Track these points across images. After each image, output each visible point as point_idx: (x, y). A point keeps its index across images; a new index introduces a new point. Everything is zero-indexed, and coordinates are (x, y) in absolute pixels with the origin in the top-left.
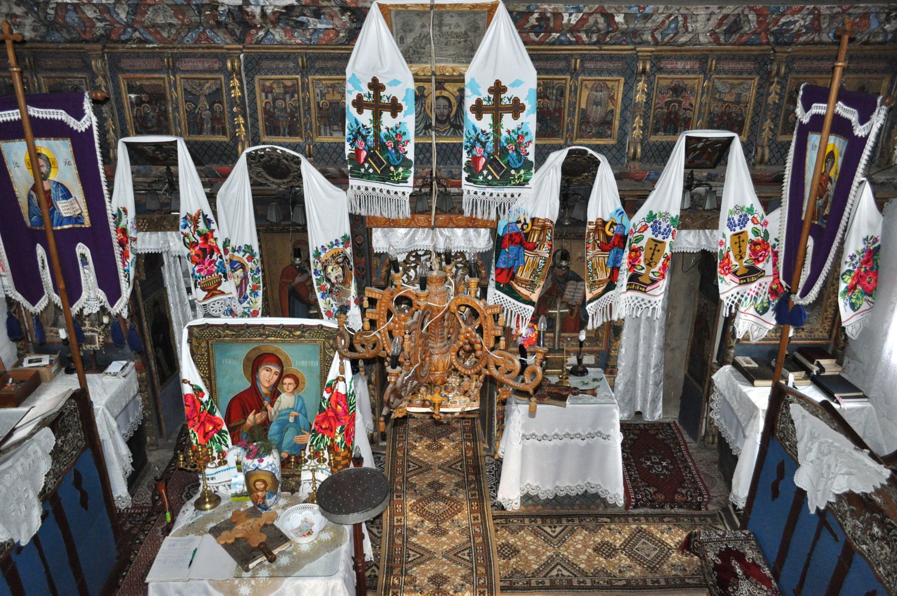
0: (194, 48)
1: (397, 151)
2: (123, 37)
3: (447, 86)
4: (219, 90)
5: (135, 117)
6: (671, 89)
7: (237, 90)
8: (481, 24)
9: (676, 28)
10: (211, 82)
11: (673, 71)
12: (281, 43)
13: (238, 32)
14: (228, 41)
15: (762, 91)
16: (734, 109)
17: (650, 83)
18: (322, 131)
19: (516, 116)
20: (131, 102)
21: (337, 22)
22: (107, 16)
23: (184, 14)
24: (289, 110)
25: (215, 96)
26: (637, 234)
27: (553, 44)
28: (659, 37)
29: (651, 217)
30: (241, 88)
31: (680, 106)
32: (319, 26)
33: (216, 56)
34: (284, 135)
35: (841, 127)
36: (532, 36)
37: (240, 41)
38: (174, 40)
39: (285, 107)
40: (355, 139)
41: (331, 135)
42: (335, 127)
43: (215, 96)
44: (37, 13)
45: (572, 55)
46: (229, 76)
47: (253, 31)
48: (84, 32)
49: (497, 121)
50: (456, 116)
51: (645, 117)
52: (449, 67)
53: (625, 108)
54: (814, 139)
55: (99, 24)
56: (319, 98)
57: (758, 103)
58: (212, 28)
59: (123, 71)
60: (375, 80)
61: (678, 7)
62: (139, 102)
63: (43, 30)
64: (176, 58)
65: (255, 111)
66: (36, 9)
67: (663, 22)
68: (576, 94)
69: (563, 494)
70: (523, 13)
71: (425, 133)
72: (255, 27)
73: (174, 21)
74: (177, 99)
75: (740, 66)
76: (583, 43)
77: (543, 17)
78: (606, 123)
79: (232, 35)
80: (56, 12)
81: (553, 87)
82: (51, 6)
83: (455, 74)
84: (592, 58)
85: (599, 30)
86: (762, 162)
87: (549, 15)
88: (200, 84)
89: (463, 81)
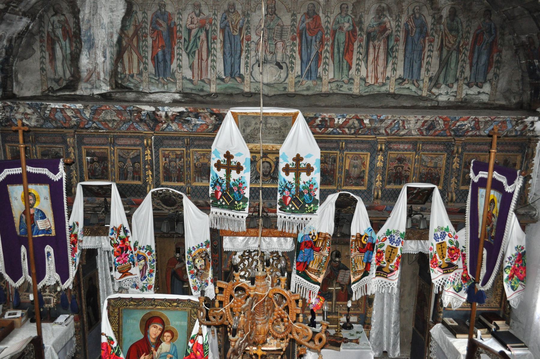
1: (239, 193)
2: (86, 126)
3: (269, 155)
4: (139, 155)
6: (397, 159)
8: (289, 123)
9: (399, 127)
11: (397, 150)
12: (175, 131)
13: (152, 125)
14: (146, 129)
15: (449, 161)
16: (433, 170)
17: (385, 156)
18: (197, 180)
20: (88, 162)
21: (208, 120)
22: (79, 115)
23: (122, 115)
24: (178, 168)
25: (136, 159)
27: (329, 134)
30: (151, 155)
32: (197, 122)
33: (138, 137)
34: (174, 181)
35: (497, 186)
36: (318, 130)
37: (153, 129)
38: (115, 128)
40: (215, 185)
41: (202, 181)
42: (204, 178)
43: (136, 159)
44: (40, 113)
46: (145, 148)
47: (160, 124)
48: (65, 123)
50: (274, 172)
51: (383, 175)
52: (270, 146)
53: (371, 170)
54: (482, 192)
55: (74, 119)
56: (195, 161)
57: (447, 168)
58: (137, 122)
59: (85, 144)
60: (228, 152)
62: (92, 161)
63: (42, 121)
64: (115, 138)
65: (159, 167)
67: (391, 124)
70: (312, 117)
71: (256, 182)
72: (161, 122)
73: (116, 118)
74: (114, 160)
75: (435, 147)
76: (346, 134)
77: (323, 120)
78: (360, 178)
79: (148, 126)
80: (50, 113)
81: (330, 157)
84: (351, 142)
85: (355, 127)
86: (451, 201)
88: (128, 152)
89: (278, 153)
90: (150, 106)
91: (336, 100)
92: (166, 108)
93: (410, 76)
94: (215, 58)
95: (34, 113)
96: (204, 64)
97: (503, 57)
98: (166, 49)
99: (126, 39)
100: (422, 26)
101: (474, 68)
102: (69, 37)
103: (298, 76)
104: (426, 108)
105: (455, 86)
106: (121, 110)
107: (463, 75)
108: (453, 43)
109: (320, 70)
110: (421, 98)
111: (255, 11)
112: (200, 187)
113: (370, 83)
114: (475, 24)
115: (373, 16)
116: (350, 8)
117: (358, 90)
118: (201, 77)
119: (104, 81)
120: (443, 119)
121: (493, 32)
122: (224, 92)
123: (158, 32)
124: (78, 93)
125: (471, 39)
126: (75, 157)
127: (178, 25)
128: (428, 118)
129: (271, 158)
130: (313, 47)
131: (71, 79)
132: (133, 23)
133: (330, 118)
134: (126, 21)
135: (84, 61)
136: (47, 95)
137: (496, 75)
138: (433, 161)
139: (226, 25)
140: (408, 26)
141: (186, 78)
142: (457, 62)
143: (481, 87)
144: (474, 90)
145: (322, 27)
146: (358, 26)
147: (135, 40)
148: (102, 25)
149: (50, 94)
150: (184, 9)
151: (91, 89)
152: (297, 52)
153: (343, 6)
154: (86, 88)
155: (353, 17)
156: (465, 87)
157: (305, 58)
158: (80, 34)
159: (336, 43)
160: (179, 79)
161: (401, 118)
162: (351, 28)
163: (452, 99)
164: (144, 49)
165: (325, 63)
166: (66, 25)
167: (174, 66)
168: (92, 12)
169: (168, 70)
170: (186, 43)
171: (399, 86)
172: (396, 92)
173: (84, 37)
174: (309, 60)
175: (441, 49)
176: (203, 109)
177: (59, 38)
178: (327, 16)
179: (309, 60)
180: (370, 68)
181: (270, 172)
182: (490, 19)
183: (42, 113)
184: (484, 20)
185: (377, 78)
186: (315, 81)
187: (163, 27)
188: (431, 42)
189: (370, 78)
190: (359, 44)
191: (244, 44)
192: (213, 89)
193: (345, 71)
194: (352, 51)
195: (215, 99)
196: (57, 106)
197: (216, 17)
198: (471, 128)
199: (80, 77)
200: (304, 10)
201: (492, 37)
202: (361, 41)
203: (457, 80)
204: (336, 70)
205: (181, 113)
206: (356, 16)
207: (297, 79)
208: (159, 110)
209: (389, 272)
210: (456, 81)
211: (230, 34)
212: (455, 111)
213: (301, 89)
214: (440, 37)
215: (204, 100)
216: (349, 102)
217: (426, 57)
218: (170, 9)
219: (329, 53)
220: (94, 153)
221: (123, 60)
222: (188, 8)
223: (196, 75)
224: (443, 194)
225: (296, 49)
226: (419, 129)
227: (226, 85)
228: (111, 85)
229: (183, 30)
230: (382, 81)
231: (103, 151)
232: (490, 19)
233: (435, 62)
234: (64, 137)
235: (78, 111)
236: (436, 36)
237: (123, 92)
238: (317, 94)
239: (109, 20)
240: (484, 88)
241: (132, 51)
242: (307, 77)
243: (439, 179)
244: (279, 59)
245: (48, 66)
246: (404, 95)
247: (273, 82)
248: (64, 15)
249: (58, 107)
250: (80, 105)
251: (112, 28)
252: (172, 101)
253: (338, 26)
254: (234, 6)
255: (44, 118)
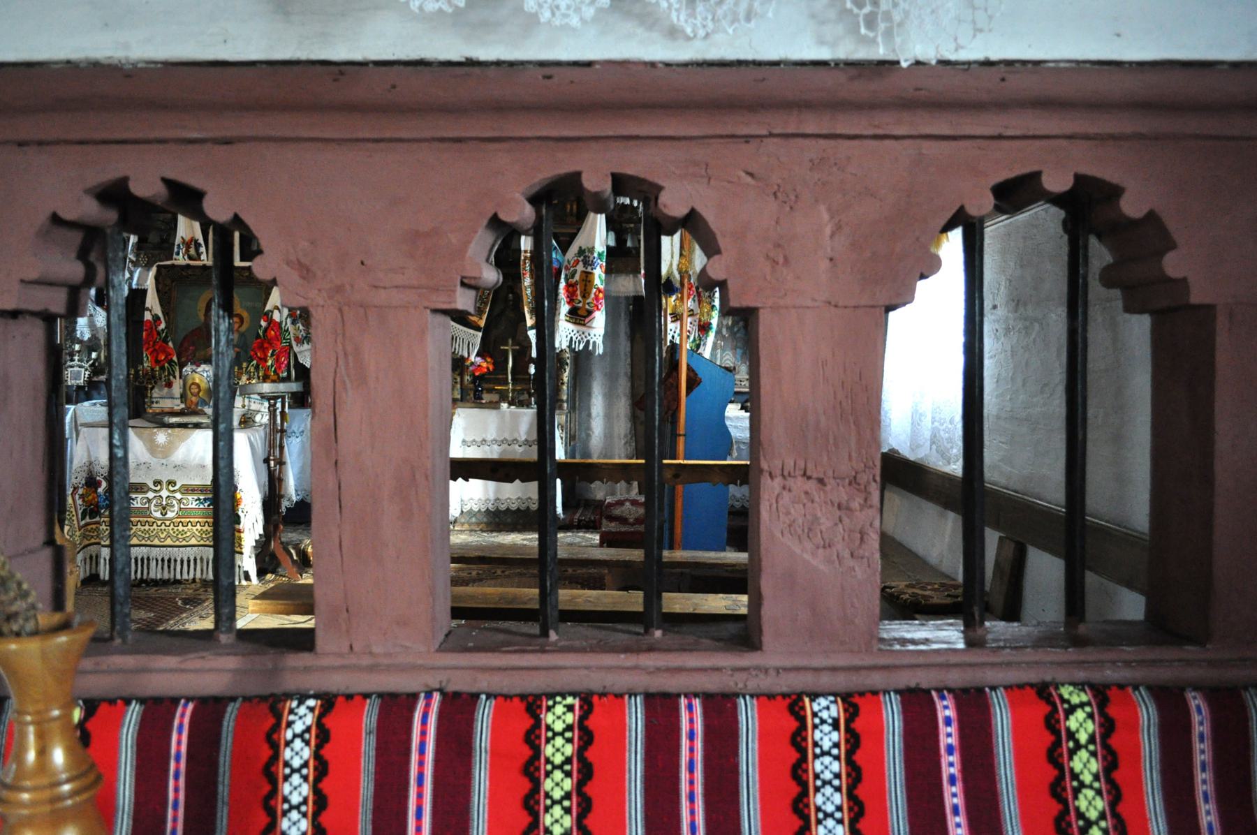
26: (572, 269)
29: (581, 252)
69: (503, 507)
209: (585, 314)
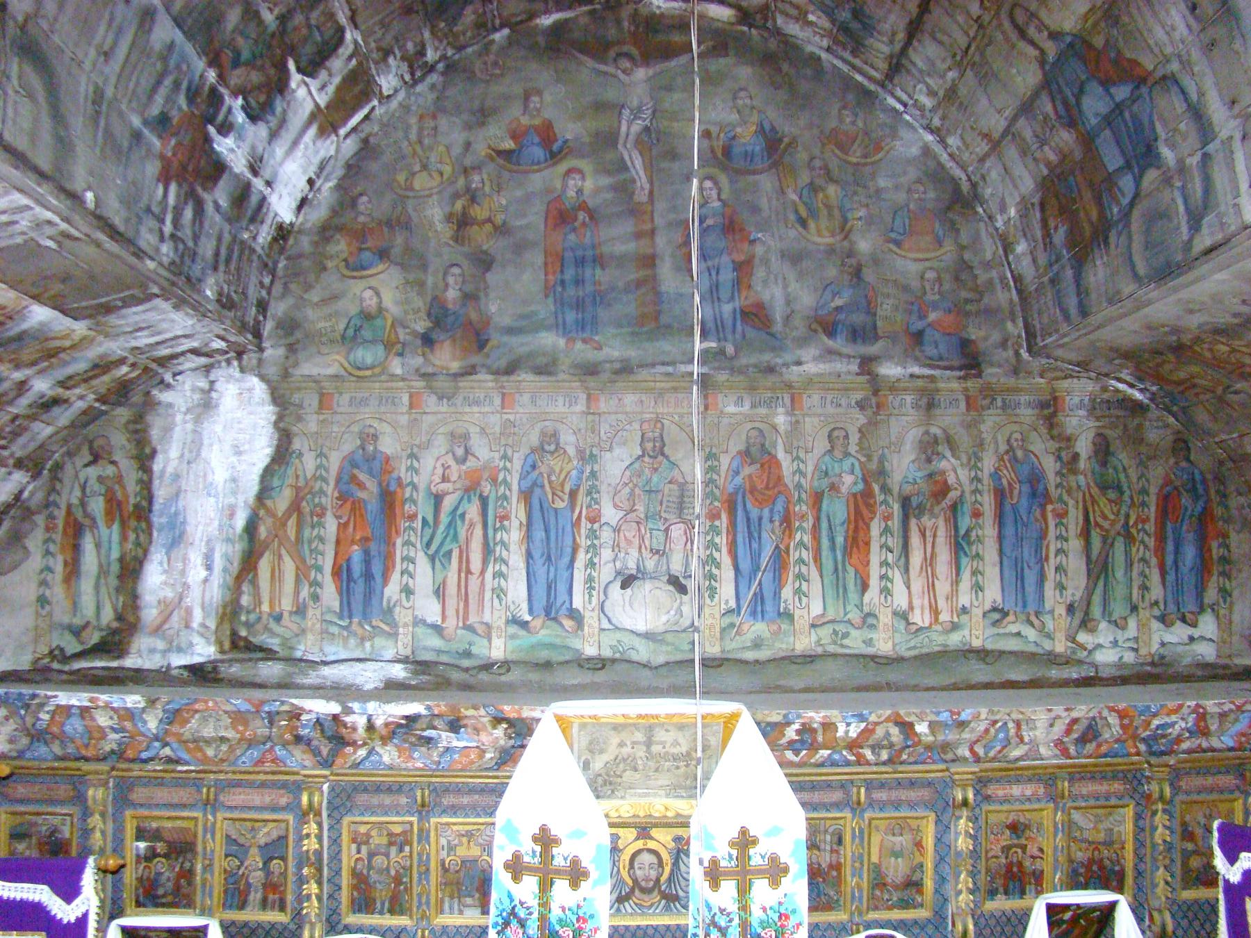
0: (250, 773)
2: (144, 755)
3: (654, 832)
4: (283, 838)
5: (140, 880)
6: (1007, 827)
7: (314, 840)
10: (271, 825)
11: (1006, 800)
12: (391, 767)
13: (325, 751)
14: (307, 763)
15: (1141, 823)
17: (974, 819)
19: (775, 883)
20: (138, 856)
21: (484, 737)
22: (128, 725)
24: (393, 873)
25: (274, 850)
27: (822, 765)
28: (980, 751)
30: (320, 838)
31: (1024, 853)
32: (455, 743)
33: (284, 785)
34: (381, 913)
36: (789, 755)
37: (327, 763)
38: (222, 761)
39: (388, 869)
40: (507, 924)
41: (461, 912)
42: (469, 901)
43: (274, 850)
44: (23, 718)
45: (852, 781)
46: (303, 816)
47: (349, 749)
48: (87, 746)
49: (744, 891)
51: (973, 874)
52: (660, 805)
53: (940, 860)
56: (445, 853)
57: (1139, 844)
58: (285, 745)
59: (134, 805)
60: (544, 829)
61: (1008, 711)
62: (151, 855)
63: (25, 741)
64: (221, 787)
65: (338, 872)
66: (23, 712)
67: (987, 731)
68: (862, 839)
72: (353, 744)
73: (230, 734)
74: (213, 851)
75: (1103, 788)
76: (868, 763)
77: (806, 729)
78: (913, 884)
79: (315, 756)
80: (53, 718)
81: (826, 831)
82: (47, 709)
83: (670, 814)
84: (882, 785)
85: (891, 745)
87: (815, 726)
88: (253, 829)
89: (686, 825)
90: (328, 699)
91: (832, 672)
92: (372, 707)
93: (1020, 604)
94: (504, 568)
95: (7, 718)
96: (474, 582)
97: (1233, 545)
98: (373, 547)
99: (269, 521)
100: (1035, 480)
101: (1171, 578)
102: (121, 516)
103: (730, 612)
104: (1066, 683)
105: (1132, 623)
106: (248, 711)
107: (1147, 596)
108: (1112, 517)
109: (787, 593)
110: (1052, 659)
111: (610, 449)
112: (458, 928)
113: (920, 624)
114: (1157, 473)
115: (913, 457)
116: (854, 438)
117: (890, 644)
118: (466, 618)
119: (201, 630)
120: (1118, 712)
121: (1201, 491)
122: (527, 659)
123: (353, 503)
124: (130, 662)
125: (1153, 509)
126: (105, 840)
127: (408, 485)
128: (1081, 711)
129: (661, 839)
130: (764, 535)
131: (115, 625)
132: (290, 480)
133: (823, 725)
134: (272, 476)
135: (154, 579)
136: (48, 669)
137: (1225, 593)
138: (1101, 826)
139: (535, 484)
140: (1000, 479)
141: (423, 622)
142: (1129, 564)
143: (1194, 625)
144: (1179, 633)
145: (786, 485)
146: (876, 481)
147: (292, 523)
148: (209, 489)
149: (55, 666)
150: (427, 445)
151: (165, 652)
152: (724, 550)
153: (836, 433)
154: (152, 651)
155: (863, 459)
156: (1155, 625)
157: (745, 565)
158: (150, 511)
159: (824, 525)
160: (406, 625)
161: (1015, 716)
162: (860, 486)
163: (1129, 657)
164: (313, 546)
165: (799, 576)
166: (117, 487)
167: (392, 590)
168: (187, 456)
169: (375, 602)
170: (426, 528)
171: (996, 630)
172: (989, 646)
173: (160, 516)
174: (756, 568)
175: (1086, 534)
176: (476, 708)
177: (93, 520)
178: (798, 458)
179: (756, 568)
180: (918, 584)
181: (658, 880)
182: (1188, 460)
183: (29, 720)
184: (1176, 463)
185: (935, 612)
186: (772, 621)
187: (370, 492)
188: (1061, 515)
189: (917, 612)
190: (883, 525)
191: (583, 531)
192: (498, 650)
193: (853, 596)
194: (867, 544)
195: (503, 678)
196: (74, 702)
197: (508, 464)
198: (1188, 730)
199: (138, 619)
200: (736, 445)
201: (1201, 503)
202: (887, 518)
203: (1134, 609)
204: (830, 593)
205: (411, 719)
206: (869, 457)
207: (727, 620)
208: (349, 711)
210: (1132, 611)
211: (545, 505)
212: (1141, 688)
213: (736, 646)
214: (1081, 506)
215: (472, 681)
216: (869, 677)
217: (1052, 555)
218: (388, 445)
219: (807, 549)
220: (158, 830)
221: (256, 575)
222: (436, 443)
223: (451, 612)
224: (1138, 911)
225: (722, 540)
226: (1059, 743)
227: (533, 639)
228: (219, 643)
229: (421, 497)
230: (949, 618)
231: (184, 824)
232: (1188, 460)
233: (1076, 565)
234: (78, 784)
235: (129, 714)
236: (1071, 503)
237: (250, 660)
238: (783, 658)
239: (227, 475)
240: (1201, 624)
241: (283, 552)
242: (754, 614)
243: (1121, 876)
244: (677, 567)
245: (58, 592)
246: (1011, 653)
247: (661, 629)
248: (113, 463)
249: (77, 703)
250: (137, 698)
251: (234, 493)
252: (382, 685)
253: (825, 483)
254: (555, 435)
255: (33, 732)
